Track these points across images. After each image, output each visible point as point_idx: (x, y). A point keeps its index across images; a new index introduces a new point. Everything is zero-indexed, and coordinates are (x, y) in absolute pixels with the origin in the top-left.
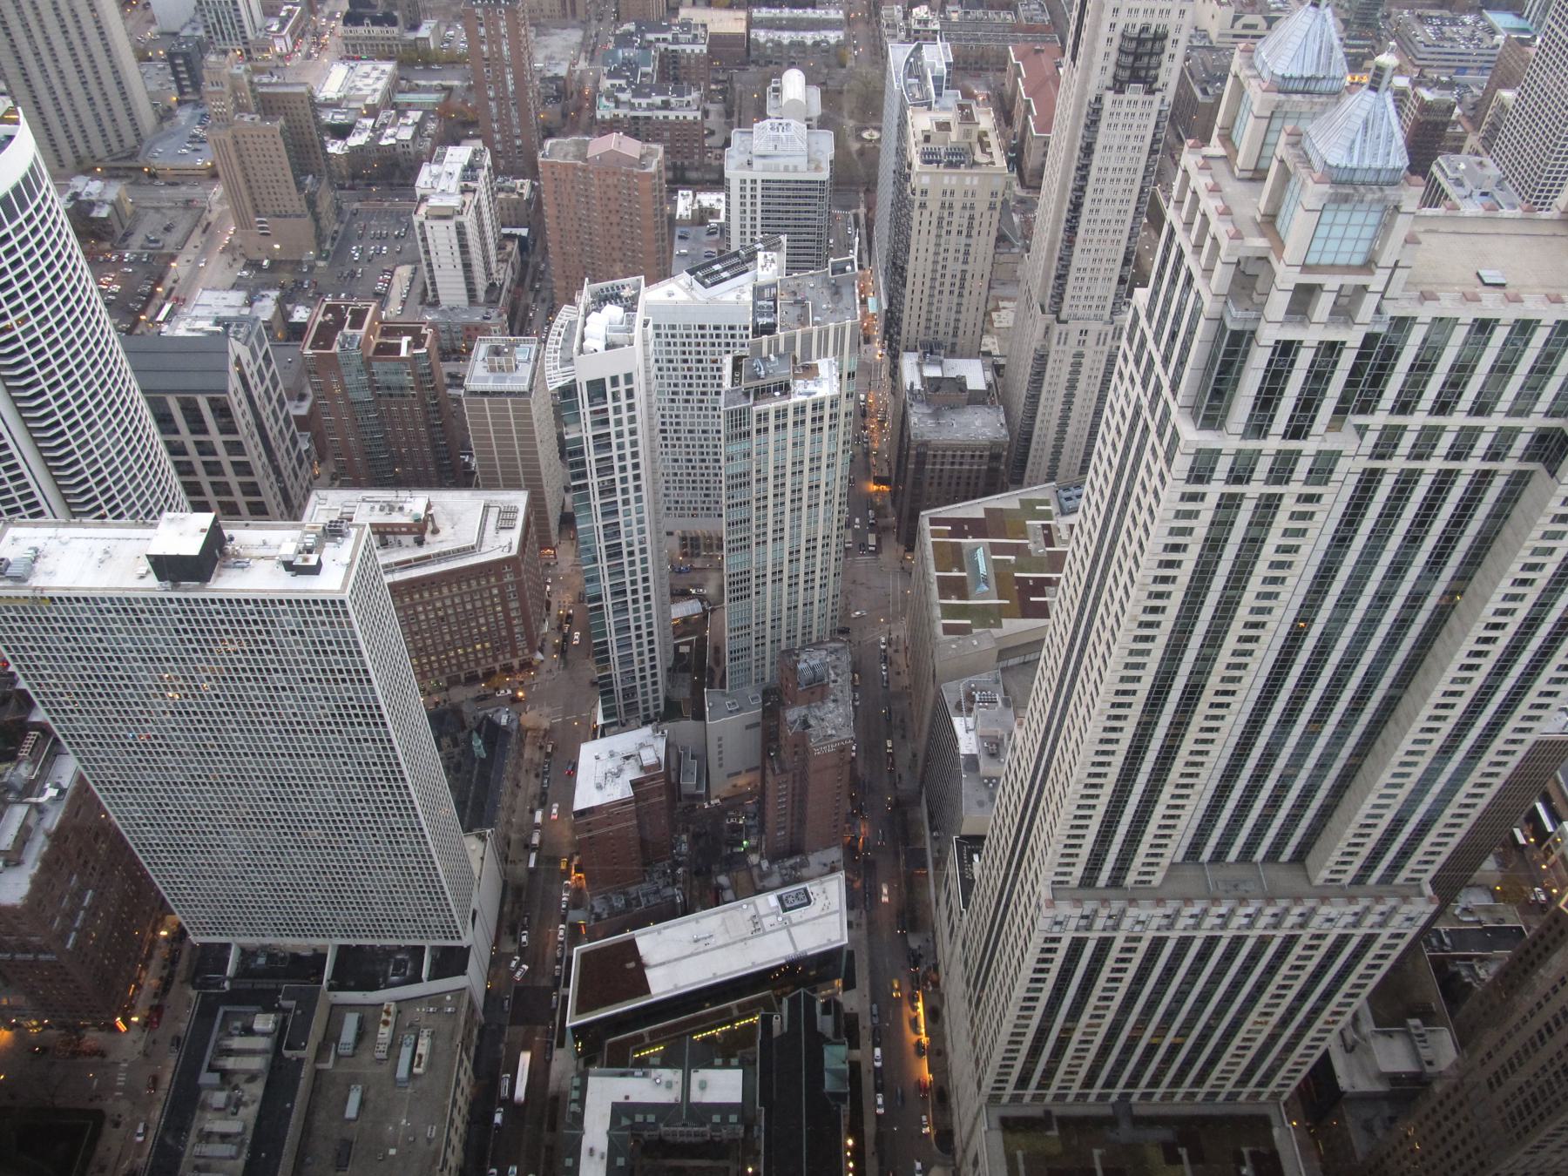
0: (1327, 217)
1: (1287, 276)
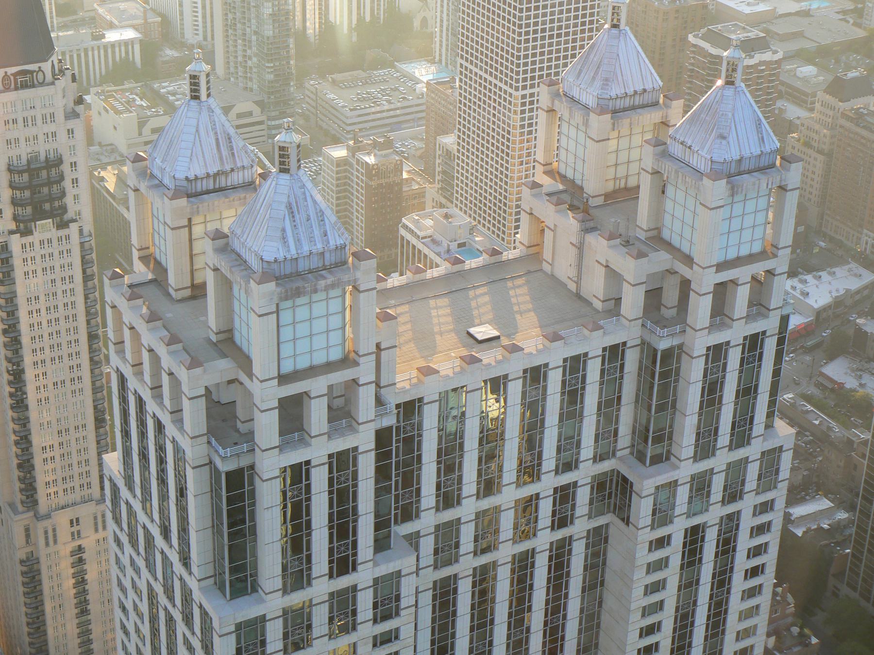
0: (286, 317)
1: (265, 394)
